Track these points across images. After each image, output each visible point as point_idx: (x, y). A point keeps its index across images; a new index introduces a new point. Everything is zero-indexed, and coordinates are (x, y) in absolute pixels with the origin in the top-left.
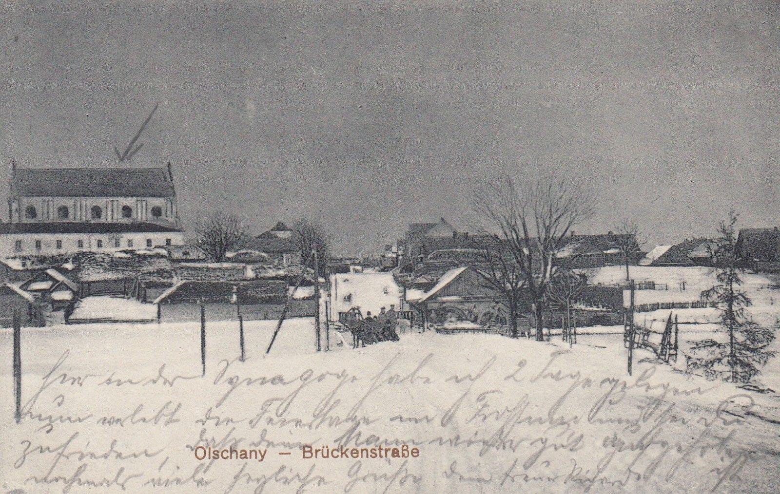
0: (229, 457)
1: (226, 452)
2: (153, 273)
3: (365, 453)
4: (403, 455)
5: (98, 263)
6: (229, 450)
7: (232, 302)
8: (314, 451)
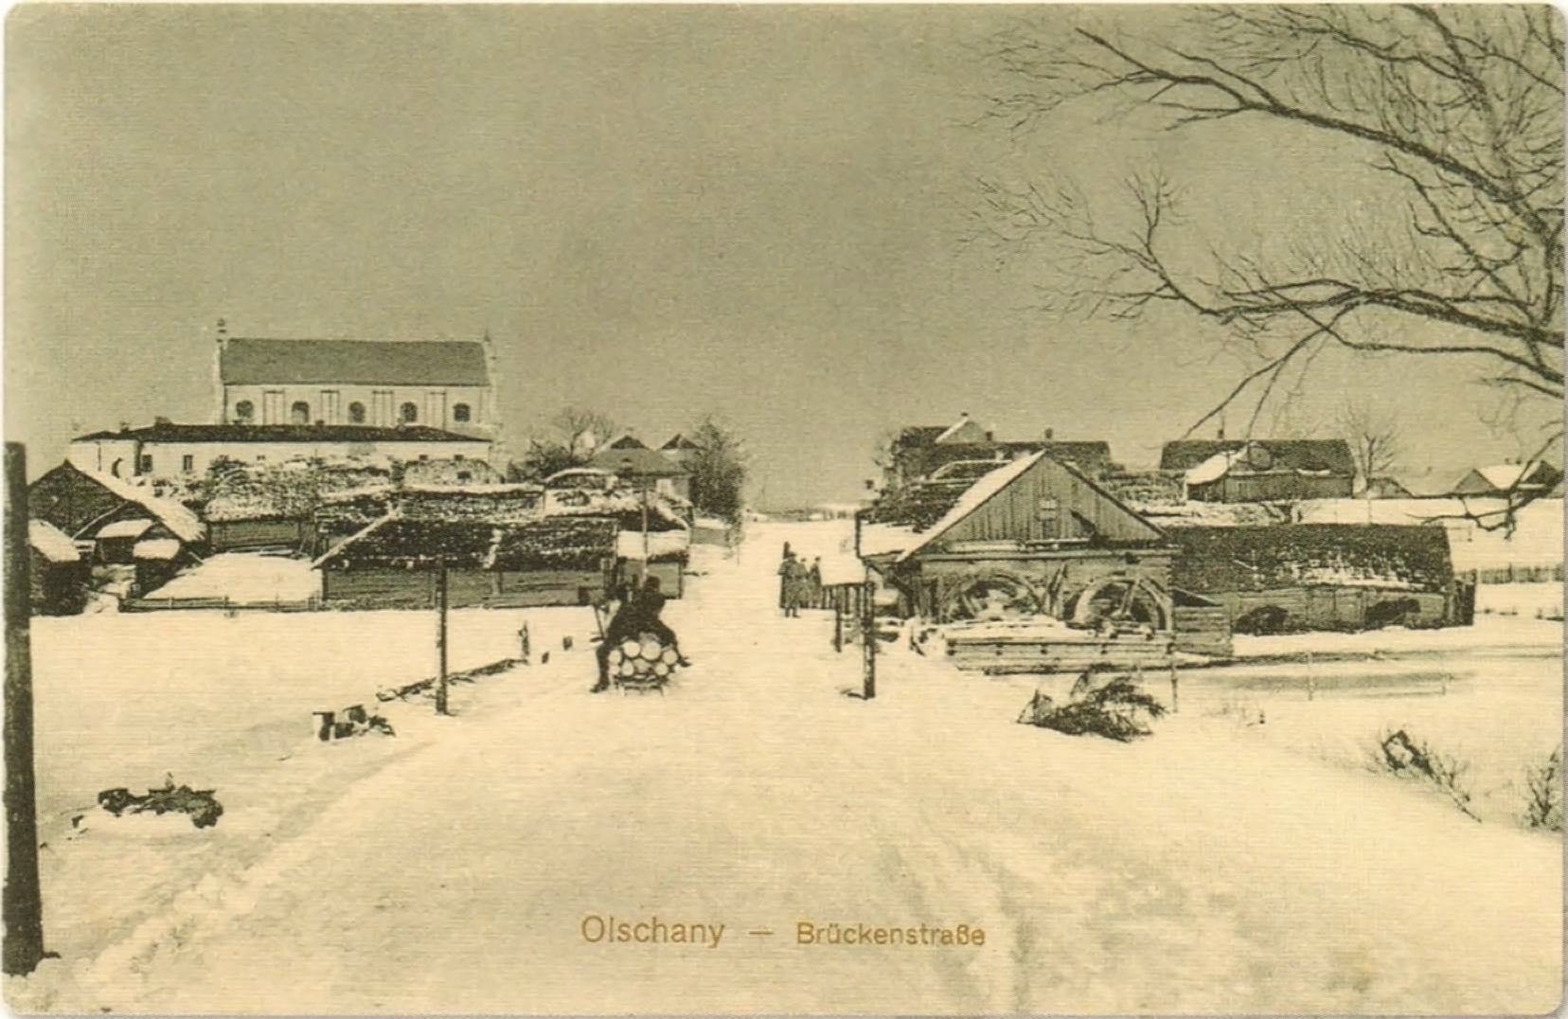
0: (651, 939)
1: (642, 928)
2: (349, 504)
3: (896, 935)
4: (959, 940)
5: (247, 485)
6: (650, 924)
7: (487, 566)
8: (814, 933)
